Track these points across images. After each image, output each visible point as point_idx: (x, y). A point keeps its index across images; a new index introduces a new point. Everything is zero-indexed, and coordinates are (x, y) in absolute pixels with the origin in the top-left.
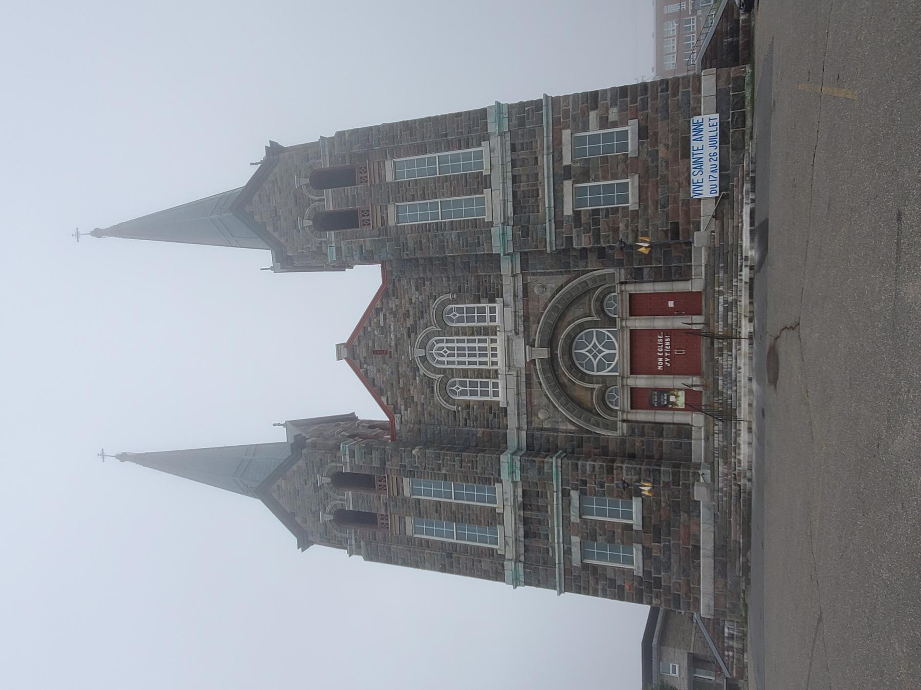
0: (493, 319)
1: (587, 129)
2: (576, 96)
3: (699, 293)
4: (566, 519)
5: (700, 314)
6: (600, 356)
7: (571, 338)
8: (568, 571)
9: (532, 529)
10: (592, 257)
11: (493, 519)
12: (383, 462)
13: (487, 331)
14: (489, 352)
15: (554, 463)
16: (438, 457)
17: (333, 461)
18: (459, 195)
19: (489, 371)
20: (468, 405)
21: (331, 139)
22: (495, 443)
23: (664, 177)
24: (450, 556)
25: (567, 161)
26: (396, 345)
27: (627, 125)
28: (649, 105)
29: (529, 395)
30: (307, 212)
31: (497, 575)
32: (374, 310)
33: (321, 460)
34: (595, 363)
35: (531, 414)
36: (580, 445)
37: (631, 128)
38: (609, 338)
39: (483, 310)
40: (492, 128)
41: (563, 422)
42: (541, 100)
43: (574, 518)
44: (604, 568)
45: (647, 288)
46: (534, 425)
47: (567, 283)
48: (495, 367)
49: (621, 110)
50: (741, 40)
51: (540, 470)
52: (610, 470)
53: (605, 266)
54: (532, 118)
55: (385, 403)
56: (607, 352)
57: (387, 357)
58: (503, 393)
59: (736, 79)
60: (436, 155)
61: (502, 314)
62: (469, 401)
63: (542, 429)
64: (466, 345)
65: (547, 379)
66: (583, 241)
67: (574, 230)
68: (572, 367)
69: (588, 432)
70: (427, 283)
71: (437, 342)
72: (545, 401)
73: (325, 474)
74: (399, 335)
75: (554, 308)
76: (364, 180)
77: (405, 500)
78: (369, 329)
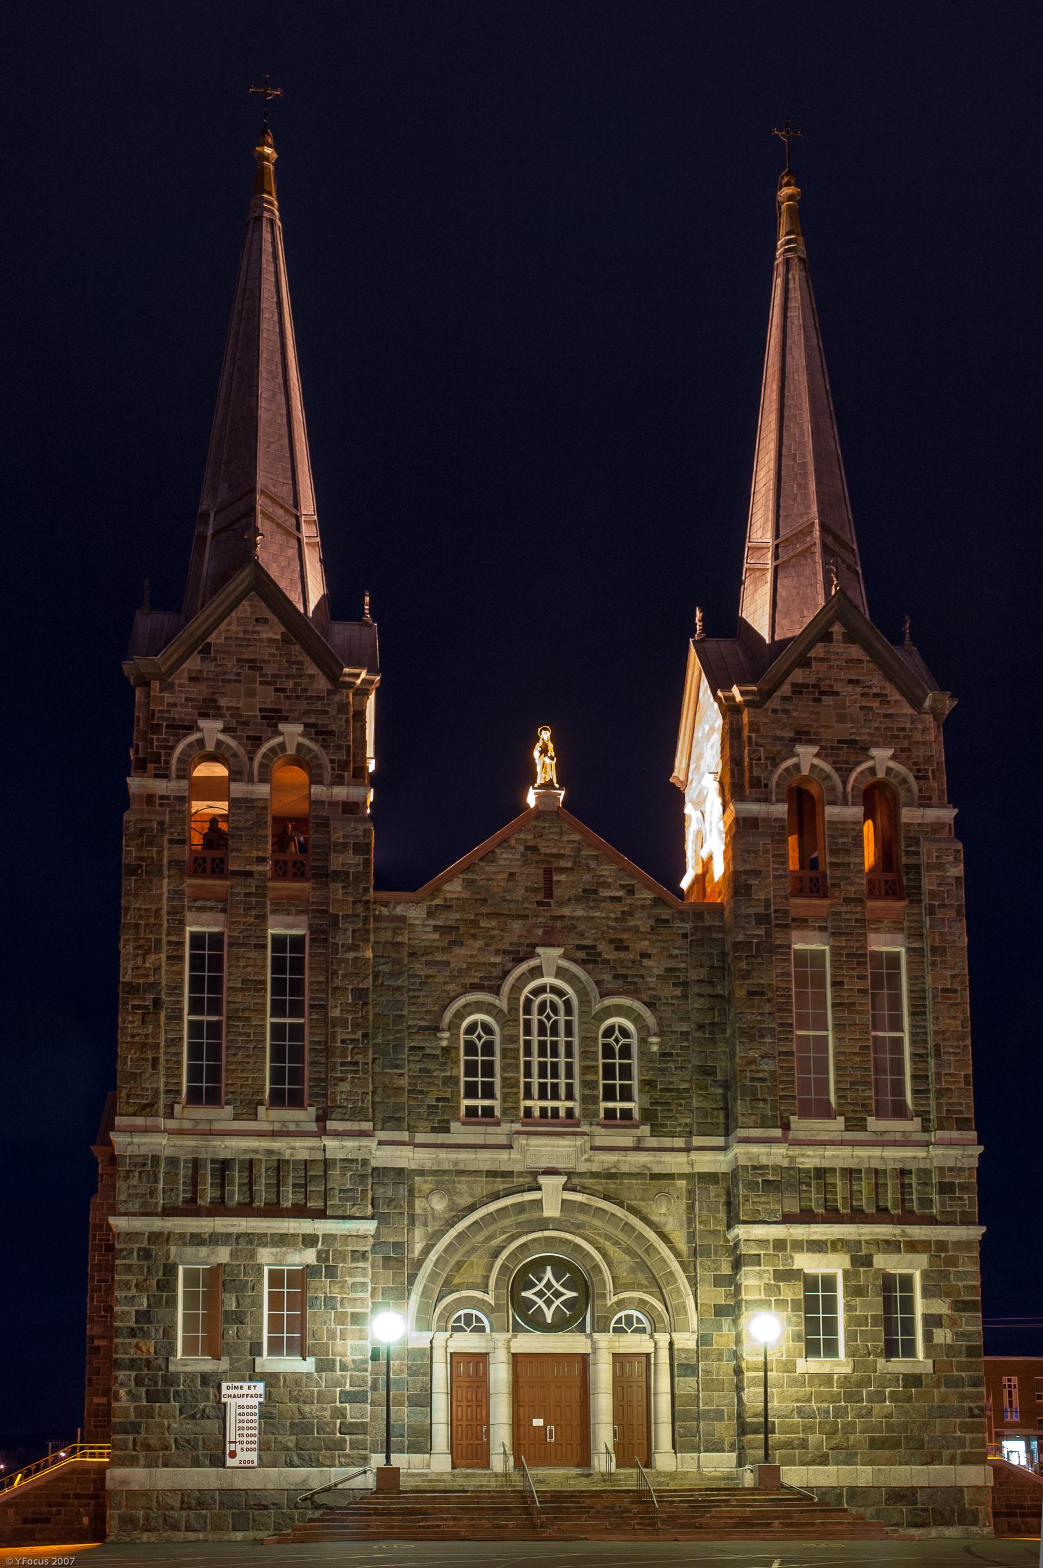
1: (926, 1293)
5: (617, 1467)
17: (332, 761)
18: (837, 1075)
27: (927, 1356)
41: (426, 1234)
42: (852, 1256)
57: (540, 897)
59: (975, 1514)
70: (678, 992)
71: (568, 1004)
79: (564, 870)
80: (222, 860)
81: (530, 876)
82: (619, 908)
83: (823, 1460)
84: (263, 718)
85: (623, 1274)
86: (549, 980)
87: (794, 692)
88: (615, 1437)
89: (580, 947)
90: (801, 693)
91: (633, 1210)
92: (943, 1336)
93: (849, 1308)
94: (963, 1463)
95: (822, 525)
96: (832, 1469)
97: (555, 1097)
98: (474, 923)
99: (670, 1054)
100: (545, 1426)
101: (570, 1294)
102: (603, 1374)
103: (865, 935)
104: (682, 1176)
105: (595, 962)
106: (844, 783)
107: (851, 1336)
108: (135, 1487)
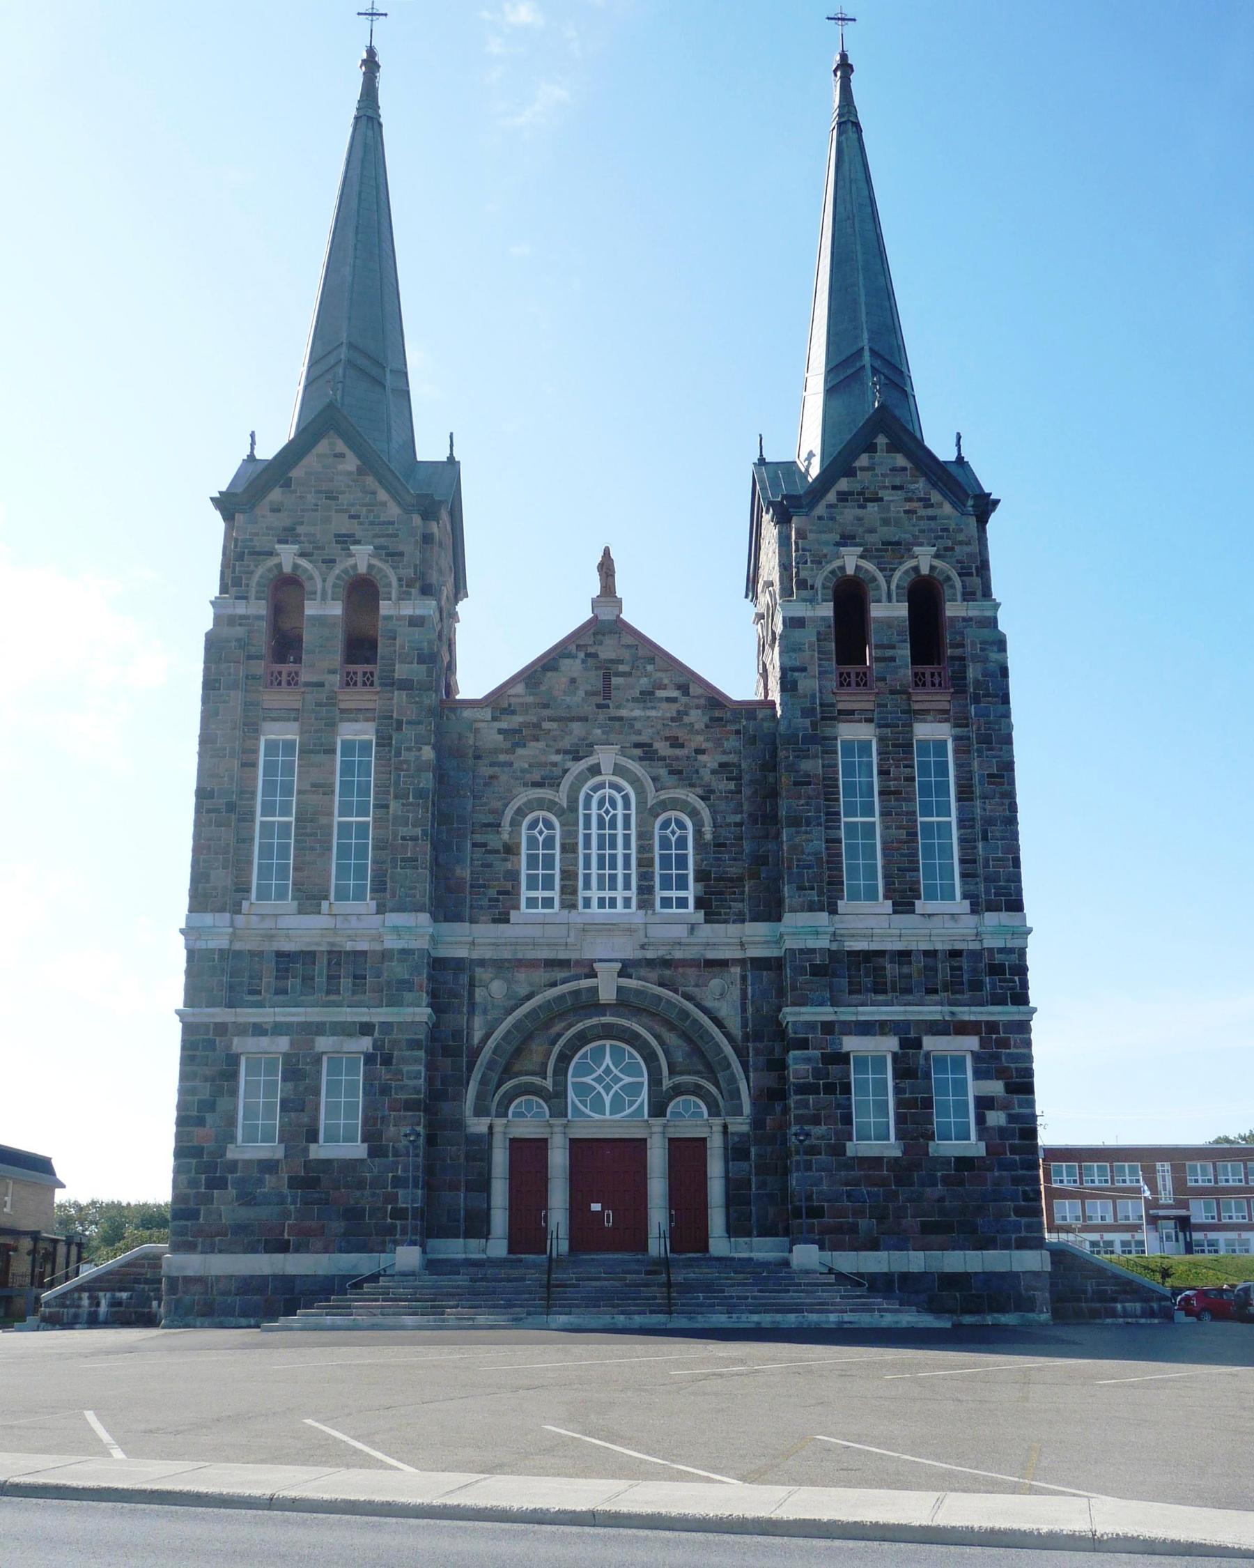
0: (666, 902)
1: (978, 1075)
2: (1030, 1058)
3: (705, 1249)
4: (319, 1029)
6: (600, 1088)
7: (633, 1039)
8: (221, 1029)
9: (293, 969)
10: (770, 1080)
11: (310, 898)
12: (406, 685)
13: (645, 890)
14: (607, 894)
15: (421, 1013)
16: (420, 794)
17: (400, 580)
19: (574, 892)
20: (510, 850)
21: (993, 622)
22: (447, 904)
23: (896, 1194)
24: (231, 807)
25: (931, 1043)
26: (620, 719)
27: (980, 1138)
28: (1004, 1173)
29: (533, 964)
30: (869, 566)
31: (202, 896)
32: (687, 680)
33: (401, 554)
34: (588, 1080)
35: (500, 966)
36: (447, 1052)
37: (974, 1146)
38: (631, 1103)
39: (682, 885)
40: (991, 918)
42: (900, 1040)
43: (323, 1043)
44: (234, 1092)
45: (715, 1168)
46: (478, 970)
47: (728, 1035)
48: (580, 903)
49: (1002, 1131)
50: (146, 1262)
51: (406, 985)
52: (409, 1105)
53: (754, 1104)
54: (1001, 988)
55: (512, 692)
56: (607, 1100)
58: (536, 920)
59: (1032, 1300)
60: (953, 819)
61: (677, 923)
62: (519, 854)
63: (472, 985)
64: (620, 851)
65: (562, 997)
66: (798, 1065)
67: (817, 1053)
68: (582, 1039)
69: (470, 1069)
70: (732, 786)
71: (626, 799)
72: (523, 992)
73: (374, 562)
74: (638, 725)
75: (685, 1014)
76: (919, 681)
77: (332, 725)
78: (650, 668)
79: (623, 674)
80: (297, 674)
81: (593, 680)
82: (674, 707)
83: (874, 1246)
84: (337, 542)
85: (679, 1057)
86: (607, 778)
87: (840, 500)
88: (671, 1221)
89: (637, 745)
90: (847, 500)
91: (689, 998)
92: (996, 1118)
93: (898, 1090)
94: (1019, 1247)
95: (871, 350)
96: (883, 1255)
97: (613, 887)
98: (537, 726)
99: (724, 845)
100: (603, 1210)
101: (608, 1060)
102: (657, 1159)
103: (911, 726)
104: (737, 962)
105: (651, 759)
106: (889, 583)
107: (900, 1119)
108: (190, 1273)
